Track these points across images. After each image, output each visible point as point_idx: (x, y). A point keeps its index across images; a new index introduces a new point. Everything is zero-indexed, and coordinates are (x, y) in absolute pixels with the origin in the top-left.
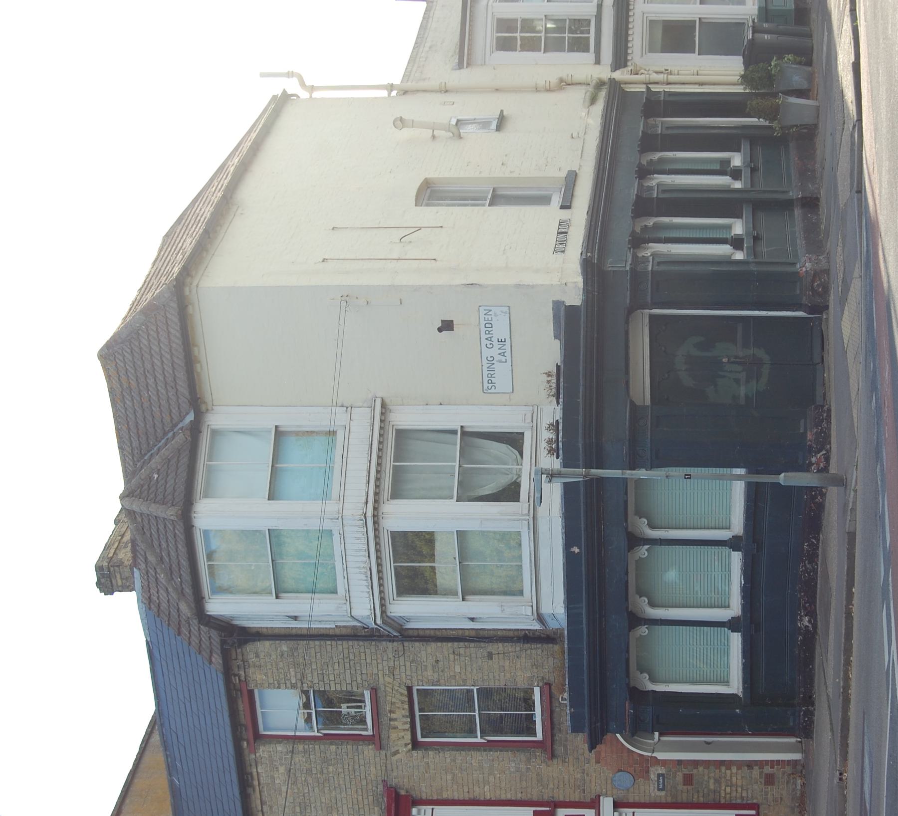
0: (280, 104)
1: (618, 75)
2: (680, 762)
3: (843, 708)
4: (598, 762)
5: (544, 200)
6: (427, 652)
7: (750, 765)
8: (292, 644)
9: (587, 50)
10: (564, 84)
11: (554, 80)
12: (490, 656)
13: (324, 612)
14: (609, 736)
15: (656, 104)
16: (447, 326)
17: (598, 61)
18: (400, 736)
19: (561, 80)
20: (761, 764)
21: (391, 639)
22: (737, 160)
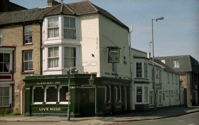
0: (127, 28)
1: (133, 82)
2: (20, 94)
3: (78, 121)
4: (20, 81)
5: (113, 71)
6: (39, 52)
7: (20, 106)
8: (40, 31)
9: (137, 77)
10: (131, 73)
11: (132, 72)
12: (38, 63)
13: (45, 36)
14: (25, 82)
15: (129, 88)
16: (93, 56)
17: (135, 79)
18: (25, 48)
19: (132, 73)
20: (20, 108)
21: (41, 47)
22: (120, 101)
